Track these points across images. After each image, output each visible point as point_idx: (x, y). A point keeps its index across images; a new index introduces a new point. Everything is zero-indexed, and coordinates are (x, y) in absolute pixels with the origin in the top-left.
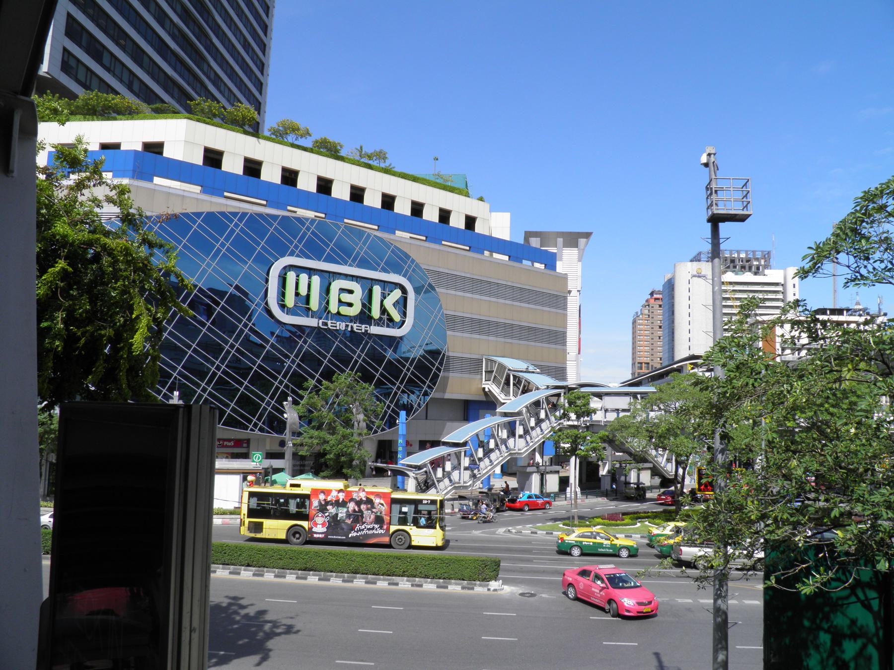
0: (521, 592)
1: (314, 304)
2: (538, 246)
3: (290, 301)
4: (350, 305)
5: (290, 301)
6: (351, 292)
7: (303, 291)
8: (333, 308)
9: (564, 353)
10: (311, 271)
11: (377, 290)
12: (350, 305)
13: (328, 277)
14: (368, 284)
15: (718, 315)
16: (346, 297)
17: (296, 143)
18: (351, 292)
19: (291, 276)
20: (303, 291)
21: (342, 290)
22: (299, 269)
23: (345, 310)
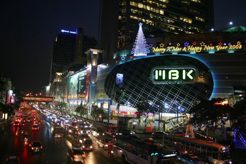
4: (175, 76)
6: (175, 73)
8: (170, 78)
12: (175, 76)
16: (173, 75)
18: (175, 73)
20: (160, 75)
21: (172, 73)
23: (173, 78)
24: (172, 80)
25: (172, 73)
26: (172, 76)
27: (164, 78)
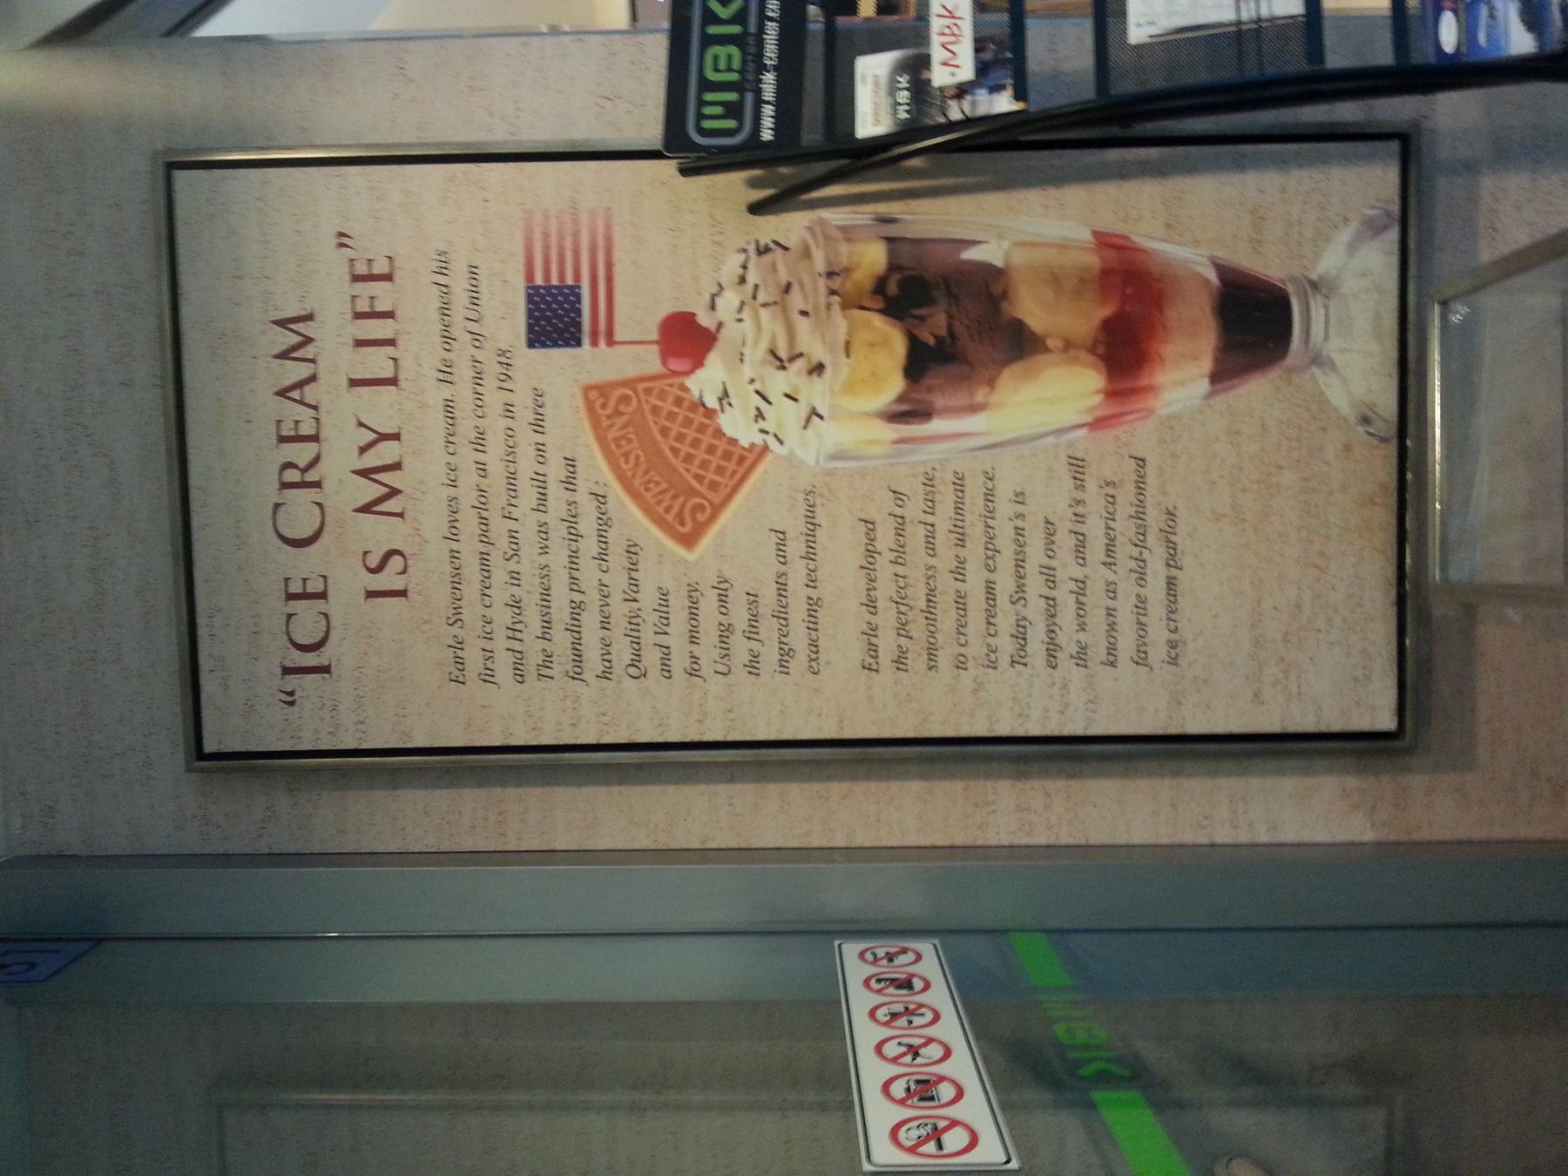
0: (895, 436)
1: (732, 96)
2: (1016, 106)
3: (730, 124)
4: (730, 57)
5: (730, 124)
6: (716, 58)
7: (718, 110)
8: (734, 77)
9: (977, 25)
10: (701, 103)
11: (713, 30)
12: (730, 57)
13: (706, 85)
14: (708, 41)
15: (724, 492)
16: (722, 66)
17: (923, 604)
18: (716, 58)
19: (707, 124)
20: (718, 110)
22: (701, 117)
23: (736, 64)
24: (741, 72)
25: (717, 70)
26: (730, 70)
27: (732, 96)
